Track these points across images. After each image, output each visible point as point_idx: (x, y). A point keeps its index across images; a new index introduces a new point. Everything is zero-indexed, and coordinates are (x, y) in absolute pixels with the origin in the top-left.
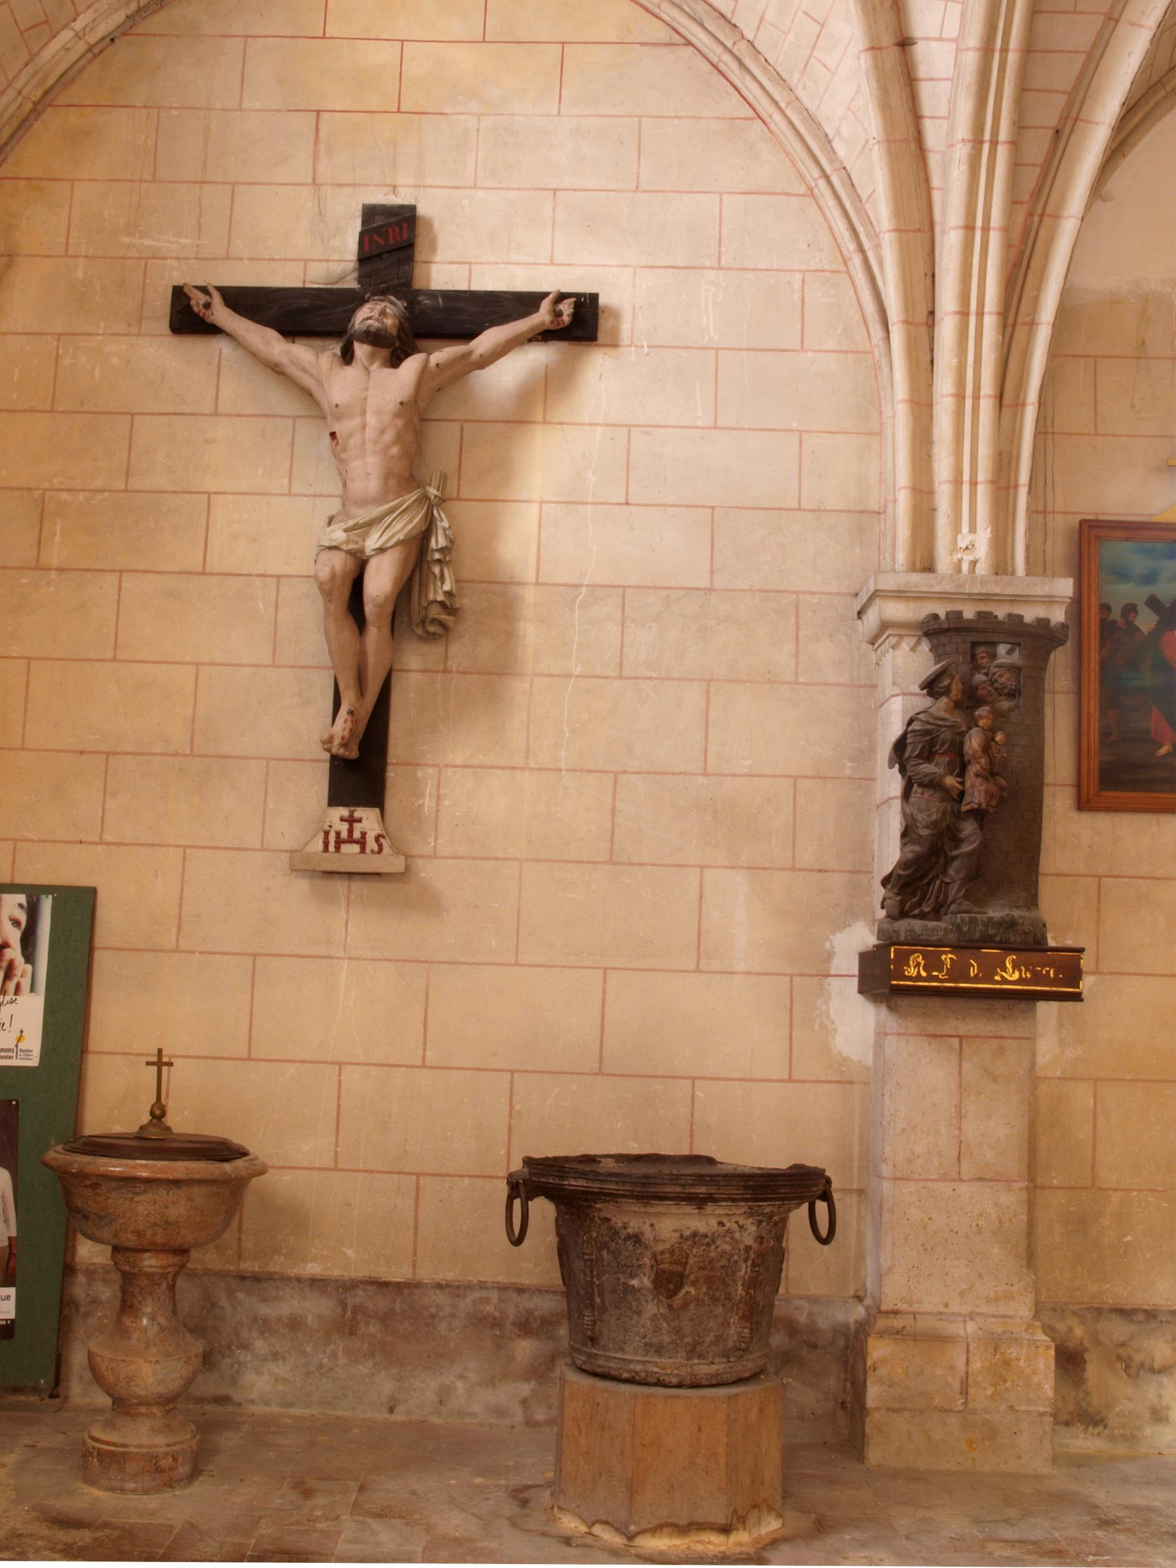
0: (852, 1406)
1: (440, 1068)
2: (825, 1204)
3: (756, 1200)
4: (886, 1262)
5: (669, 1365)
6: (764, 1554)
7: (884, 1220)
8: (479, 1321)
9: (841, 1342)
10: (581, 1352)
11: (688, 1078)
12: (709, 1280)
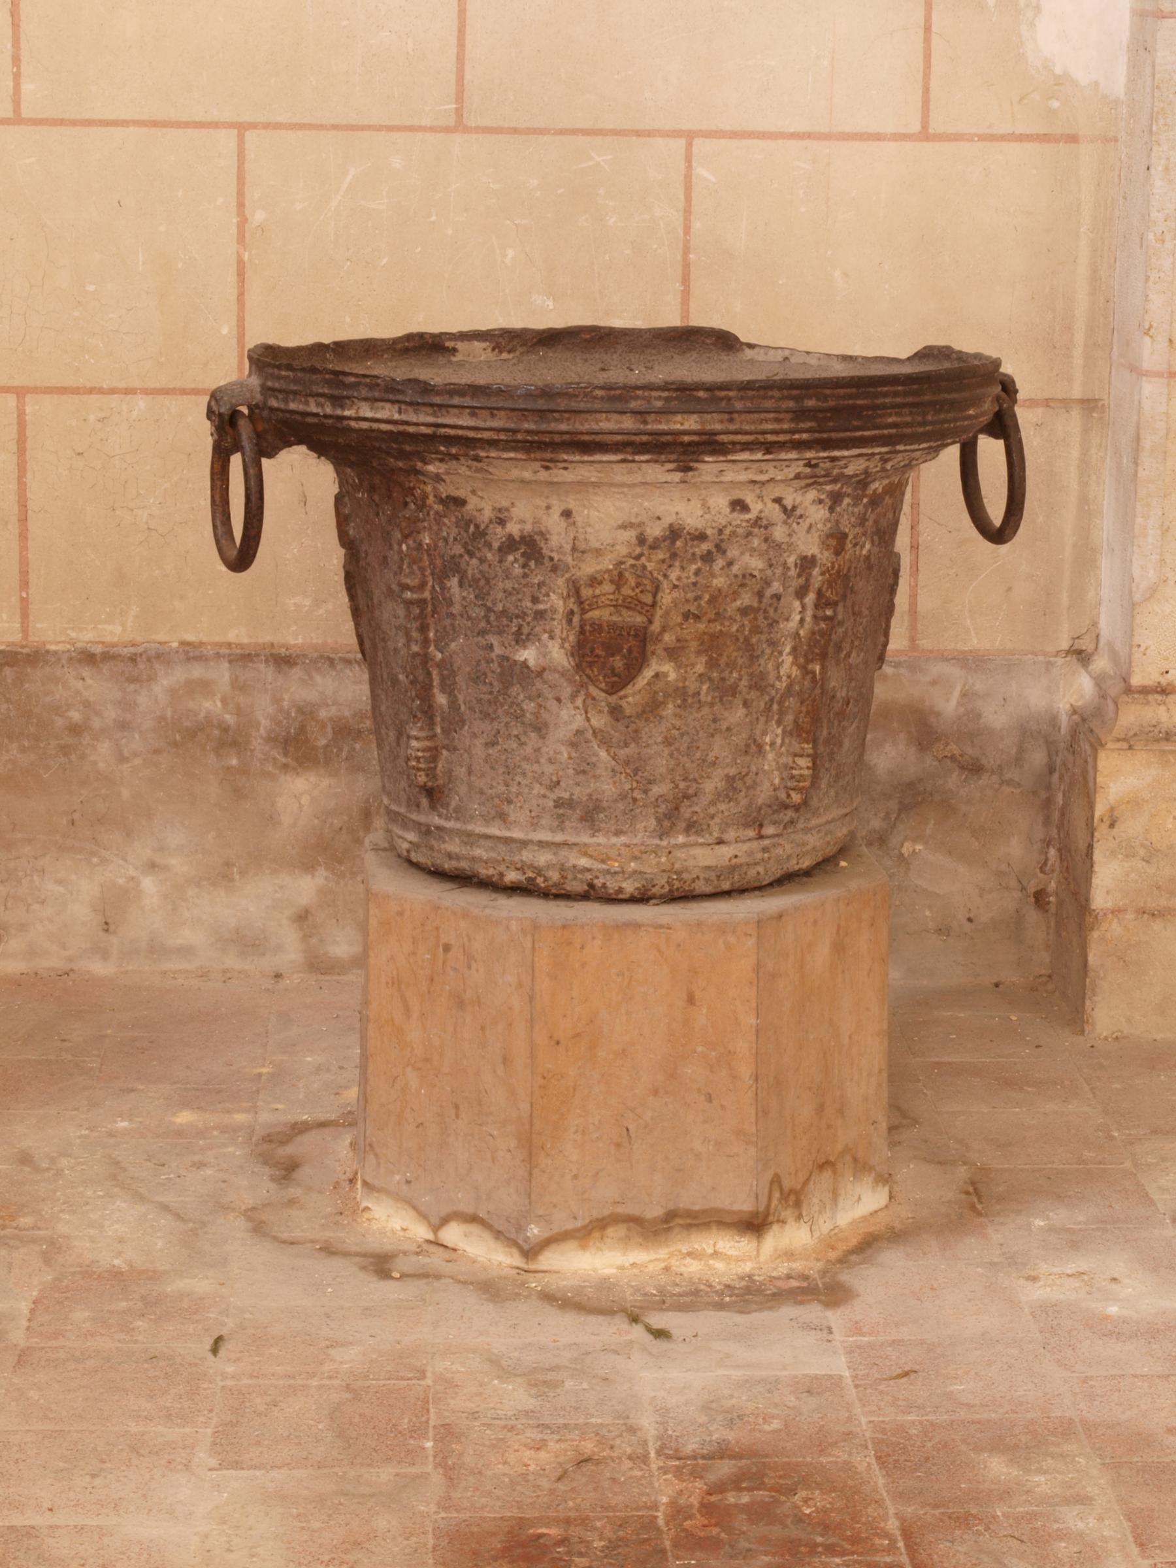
0: (1060, 902)
1: (60, 122)
2: (1000, 444)
3: (826, 445)
4: (1145, 572)
5: (617, 850)
6: (845, 1277)
7: (1141, 473)
8: (188, 737)
9: (1038, 757)
10: (405, 823)
11: (675, 134)
12: (711, 645)
